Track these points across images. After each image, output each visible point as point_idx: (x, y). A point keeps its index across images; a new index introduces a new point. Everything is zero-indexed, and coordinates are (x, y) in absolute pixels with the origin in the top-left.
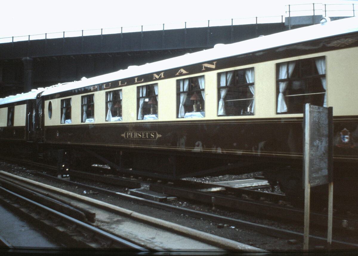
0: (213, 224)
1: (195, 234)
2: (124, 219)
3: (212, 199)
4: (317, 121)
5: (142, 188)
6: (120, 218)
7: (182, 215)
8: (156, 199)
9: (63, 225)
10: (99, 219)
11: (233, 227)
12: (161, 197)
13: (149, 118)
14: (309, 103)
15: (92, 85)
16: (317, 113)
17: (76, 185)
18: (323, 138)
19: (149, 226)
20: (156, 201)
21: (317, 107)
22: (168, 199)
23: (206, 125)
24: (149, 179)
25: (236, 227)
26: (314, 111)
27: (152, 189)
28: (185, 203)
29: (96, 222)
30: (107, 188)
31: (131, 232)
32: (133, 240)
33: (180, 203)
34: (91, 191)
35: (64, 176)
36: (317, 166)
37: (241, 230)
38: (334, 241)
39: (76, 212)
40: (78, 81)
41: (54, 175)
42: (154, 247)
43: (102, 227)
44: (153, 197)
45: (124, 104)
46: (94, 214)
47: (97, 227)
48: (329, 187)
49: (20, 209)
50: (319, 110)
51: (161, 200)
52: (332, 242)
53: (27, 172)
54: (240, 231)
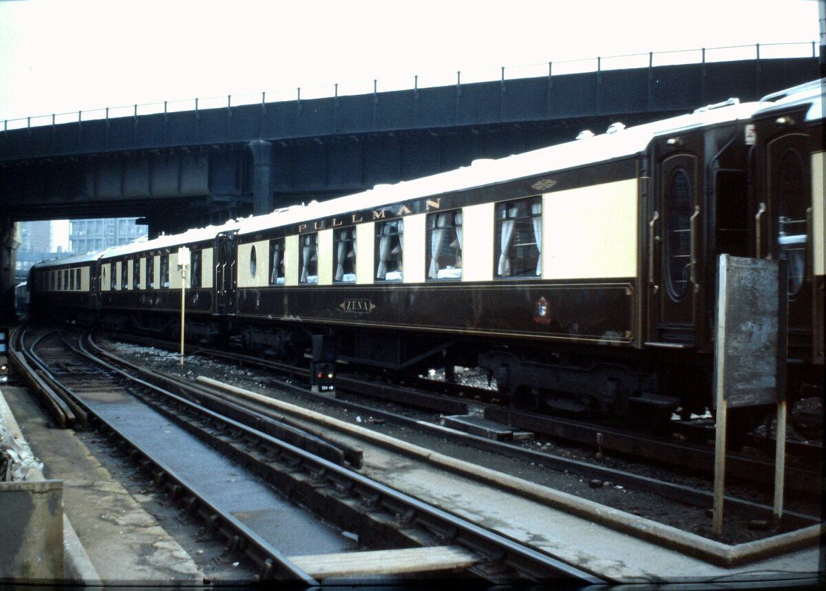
0: (584, 481)
1: (531, 491)
2: (417, 464)
3: (598, 437)
4: (750, 286)
5: (471, 414)
6: (408, 462)
7: (533, 464)
8: (491, 435)
9: (305, 471)
10: (369, 463)
11: (620, 487)
12: (501, 432)
13: (448, 273)
14: (726, 253)
15: (401, 200)
16: (750, 272)
17: (345, 406)
18: (764, 319)
19: (457, 477)
20: (491, 438)
21: (749, 260)
22: (516, 436)
23: (530, 291)
24: (494, 399)
25: (625, 488)
26: (741, 269)
27: (489, 416)
28: (549, 444)
29: (363, 468)
30: (404, 414)
31: (422, 484)
32: (421, 497)
33: (539, 444)
34: (371, 418)
35: (324, 388)
36: (748, 370)
37: (632, 492)
38: (787, 512)
39: (327, 448)
40: (394, 185)
41: (305, 388)
42: (453, 509)
43: (372, 476)
44: (486, 430)
45: (155, 279)
46: (360, 454)
47: (365, 475)
48: (779, 410)
49: (230, 444)
50: (753, 266)
51: (501, 438)
52: (784, 515)
53: (253, 381)
54: (630, 493)
